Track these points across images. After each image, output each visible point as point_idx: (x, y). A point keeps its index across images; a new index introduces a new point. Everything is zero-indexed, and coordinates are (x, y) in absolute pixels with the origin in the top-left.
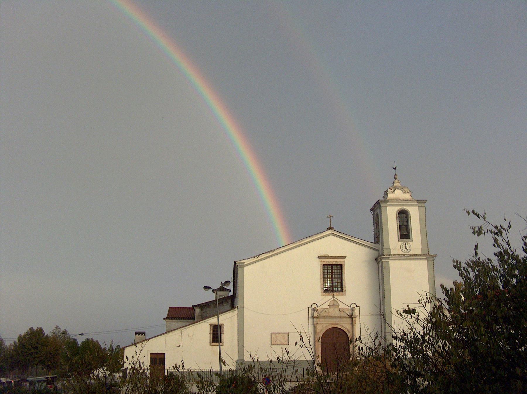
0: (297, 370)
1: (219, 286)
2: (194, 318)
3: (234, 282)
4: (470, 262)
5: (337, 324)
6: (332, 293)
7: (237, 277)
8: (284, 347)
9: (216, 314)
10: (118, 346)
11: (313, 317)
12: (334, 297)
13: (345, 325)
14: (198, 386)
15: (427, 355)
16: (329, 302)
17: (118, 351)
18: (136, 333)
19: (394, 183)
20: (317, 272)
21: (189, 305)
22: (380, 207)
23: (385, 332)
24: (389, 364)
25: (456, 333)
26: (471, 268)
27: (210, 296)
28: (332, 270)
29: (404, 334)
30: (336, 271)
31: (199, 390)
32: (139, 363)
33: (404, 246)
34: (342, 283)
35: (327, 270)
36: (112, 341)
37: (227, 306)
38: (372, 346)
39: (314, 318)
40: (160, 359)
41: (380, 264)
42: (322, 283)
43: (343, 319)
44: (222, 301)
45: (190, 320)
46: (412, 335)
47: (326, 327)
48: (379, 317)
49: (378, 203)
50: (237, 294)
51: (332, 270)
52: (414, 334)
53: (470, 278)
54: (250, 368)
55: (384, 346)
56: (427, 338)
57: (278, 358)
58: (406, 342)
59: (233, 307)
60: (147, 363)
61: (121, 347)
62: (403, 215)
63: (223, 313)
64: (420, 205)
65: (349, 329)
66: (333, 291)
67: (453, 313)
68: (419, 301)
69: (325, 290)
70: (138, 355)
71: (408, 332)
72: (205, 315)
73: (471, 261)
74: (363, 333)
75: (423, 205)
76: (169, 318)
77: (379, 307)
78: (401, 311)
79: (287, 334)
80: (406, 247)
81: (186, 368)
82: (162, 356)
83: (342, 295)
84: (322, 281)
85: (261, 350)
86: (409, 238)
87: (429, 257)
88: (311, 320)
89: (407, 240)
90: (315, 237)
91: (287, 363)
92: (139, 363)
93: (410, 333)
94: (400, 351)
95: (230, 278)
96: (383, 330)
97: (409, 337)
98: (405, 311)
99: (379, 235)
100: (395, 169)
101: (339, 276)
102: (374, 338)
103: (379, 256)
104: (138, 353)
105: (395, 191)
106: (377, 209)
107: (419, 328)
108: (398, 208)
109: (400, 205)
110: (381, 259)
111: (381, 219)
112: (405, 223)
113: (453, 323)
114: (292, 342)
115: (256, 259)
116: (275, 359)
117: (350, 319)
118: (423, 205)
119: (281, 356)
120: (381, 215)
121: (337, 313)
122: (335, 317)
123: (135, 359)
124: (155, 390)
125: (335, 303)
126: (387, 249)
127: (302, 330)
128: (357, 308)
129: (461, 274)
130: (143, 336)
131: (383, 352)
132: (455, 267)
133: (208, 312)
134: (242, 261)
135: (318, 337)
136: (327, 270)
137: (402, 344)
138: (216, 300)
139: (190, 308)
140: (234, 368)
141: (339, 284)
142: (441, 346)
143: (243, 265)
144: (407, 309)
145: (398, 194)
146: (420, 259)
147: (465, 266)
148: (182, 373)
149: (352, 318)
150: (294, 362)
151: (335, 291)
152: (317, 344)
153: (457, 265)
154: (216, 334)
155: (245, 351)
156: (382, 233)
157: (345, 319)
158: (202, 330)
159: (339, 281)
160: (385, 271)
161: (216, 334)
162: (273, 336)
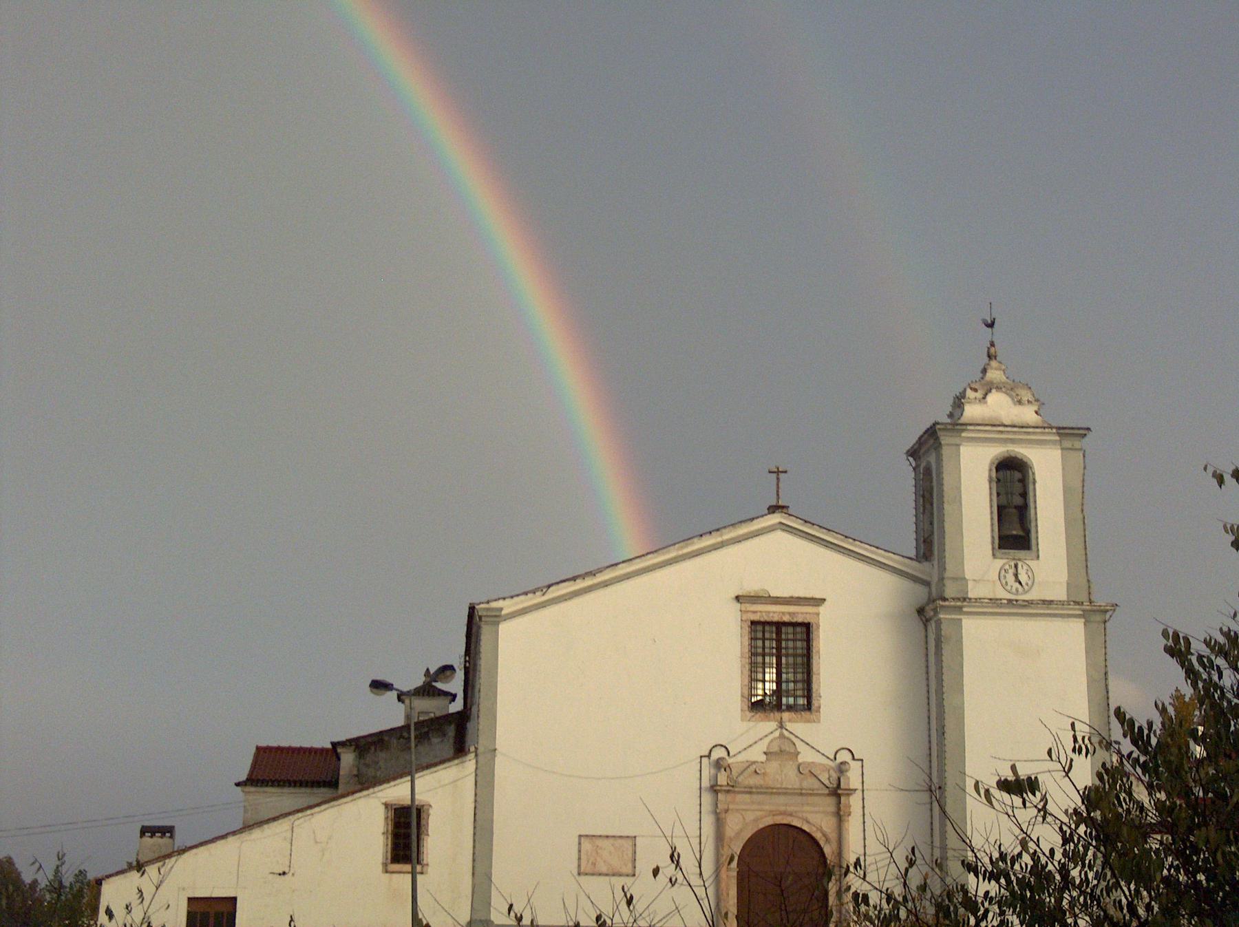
1: (419, 681)
4: (1222, 639)
5: (791, 815)
6: (778, 715)
7: (478, 653)
8: (618, 882)
9: (408, 771)
11: (714, 789)
12: (781, 726)
13: (815, 818)
16: (767, 740)
17: (81, 890)
18: (144, 831)
19: (984, 371)
20: (731, 643)
21: (322, 741)
22: (938, 446)
23: (944, 848)
26: (1226, 656)
27: (389, 714)
28: (779, 641)
29: (1003, 857)
30: (791, 644)
33: (1012, 571)
34: (808, 682)
35: (764, 639)
36: (61, 857)
37: (443, 745)
38: (898, 891)
39: (716, 792)
40: (219, 916)
42: (746, 681)
43: (810, 799)
45: (323, 790)
46: (1026, 858)
47: (756, 820)
48: (925, 797)
50: (474, 709)
51: (779, 641)
52: (1034, 856)
53: (1222, 689)
55: (938, 892)
57: (598, 918)
58: (1009, 882)
59: (460, 749)
61: (91, 876)
62: (1012, 476)
63: (428, 767)
64: (1068, 443)
66: (778, 707)
67: (1162, 796)
68: (1050, 752)
69: (753, 704)
70: (146, 903)
71: (1016, 852)
72: (371, 772)
73: (1227, 634)
74: (874, 843)
77: (925, 766)
78: (992, 782)
79: (630, 842)
80: (1016, 575)
82: (224, 908)
83: (808, 721)
84: (747, 673)
87: (1094, 612)
88: (707, 798)
90: (728, 535)
93: (1020, 855)
94: (987, 911)
96: (937, 843)
97: (1017, 867)
98: (1004, 785)
99: (932, 533)
102: (903, 865)
103: (931, 600)
105: (990, 398)
106: (927, 451)
107: (1048, 837)
108: (994, 452)
109: (1006, 441)
111: (941, 484)
112: (1018, 501)
113: (1161, 827)
114: (644, 868)
115: (538, 598)
117: (831, 801)
118: (1077, 444)
119: (607, 911)
120: (940, 473)
121: (787, 776)
122: (784, 792)
125: (787, 747)
126: (955, 579)
127: (678, 831)
128: (855, 766)
129: (1191, 674)
131: (931, 910)
132: (1171, 651)
133: (381, 764)
134: (494, 605)
135: (726, 853)
136: (764, 639)
137: (993, 888)
138: (406, 727)
139: (323, 750)
141: (800, 685)
142: (1124, 901)
143: (497, 618)
144: (1011, 778)
145: (998, 406)
147: (1205, 651)
149: (839, 796)
151: (790, 708)
152: (723, 874)
153: (1177, 649)
154: (405, 836)
155: (494, 892)
156: (942, 528)
157: (816, 799)
158: (362, 818)
159: (799, 676)
161: (405, 836)
162: (586, 845)
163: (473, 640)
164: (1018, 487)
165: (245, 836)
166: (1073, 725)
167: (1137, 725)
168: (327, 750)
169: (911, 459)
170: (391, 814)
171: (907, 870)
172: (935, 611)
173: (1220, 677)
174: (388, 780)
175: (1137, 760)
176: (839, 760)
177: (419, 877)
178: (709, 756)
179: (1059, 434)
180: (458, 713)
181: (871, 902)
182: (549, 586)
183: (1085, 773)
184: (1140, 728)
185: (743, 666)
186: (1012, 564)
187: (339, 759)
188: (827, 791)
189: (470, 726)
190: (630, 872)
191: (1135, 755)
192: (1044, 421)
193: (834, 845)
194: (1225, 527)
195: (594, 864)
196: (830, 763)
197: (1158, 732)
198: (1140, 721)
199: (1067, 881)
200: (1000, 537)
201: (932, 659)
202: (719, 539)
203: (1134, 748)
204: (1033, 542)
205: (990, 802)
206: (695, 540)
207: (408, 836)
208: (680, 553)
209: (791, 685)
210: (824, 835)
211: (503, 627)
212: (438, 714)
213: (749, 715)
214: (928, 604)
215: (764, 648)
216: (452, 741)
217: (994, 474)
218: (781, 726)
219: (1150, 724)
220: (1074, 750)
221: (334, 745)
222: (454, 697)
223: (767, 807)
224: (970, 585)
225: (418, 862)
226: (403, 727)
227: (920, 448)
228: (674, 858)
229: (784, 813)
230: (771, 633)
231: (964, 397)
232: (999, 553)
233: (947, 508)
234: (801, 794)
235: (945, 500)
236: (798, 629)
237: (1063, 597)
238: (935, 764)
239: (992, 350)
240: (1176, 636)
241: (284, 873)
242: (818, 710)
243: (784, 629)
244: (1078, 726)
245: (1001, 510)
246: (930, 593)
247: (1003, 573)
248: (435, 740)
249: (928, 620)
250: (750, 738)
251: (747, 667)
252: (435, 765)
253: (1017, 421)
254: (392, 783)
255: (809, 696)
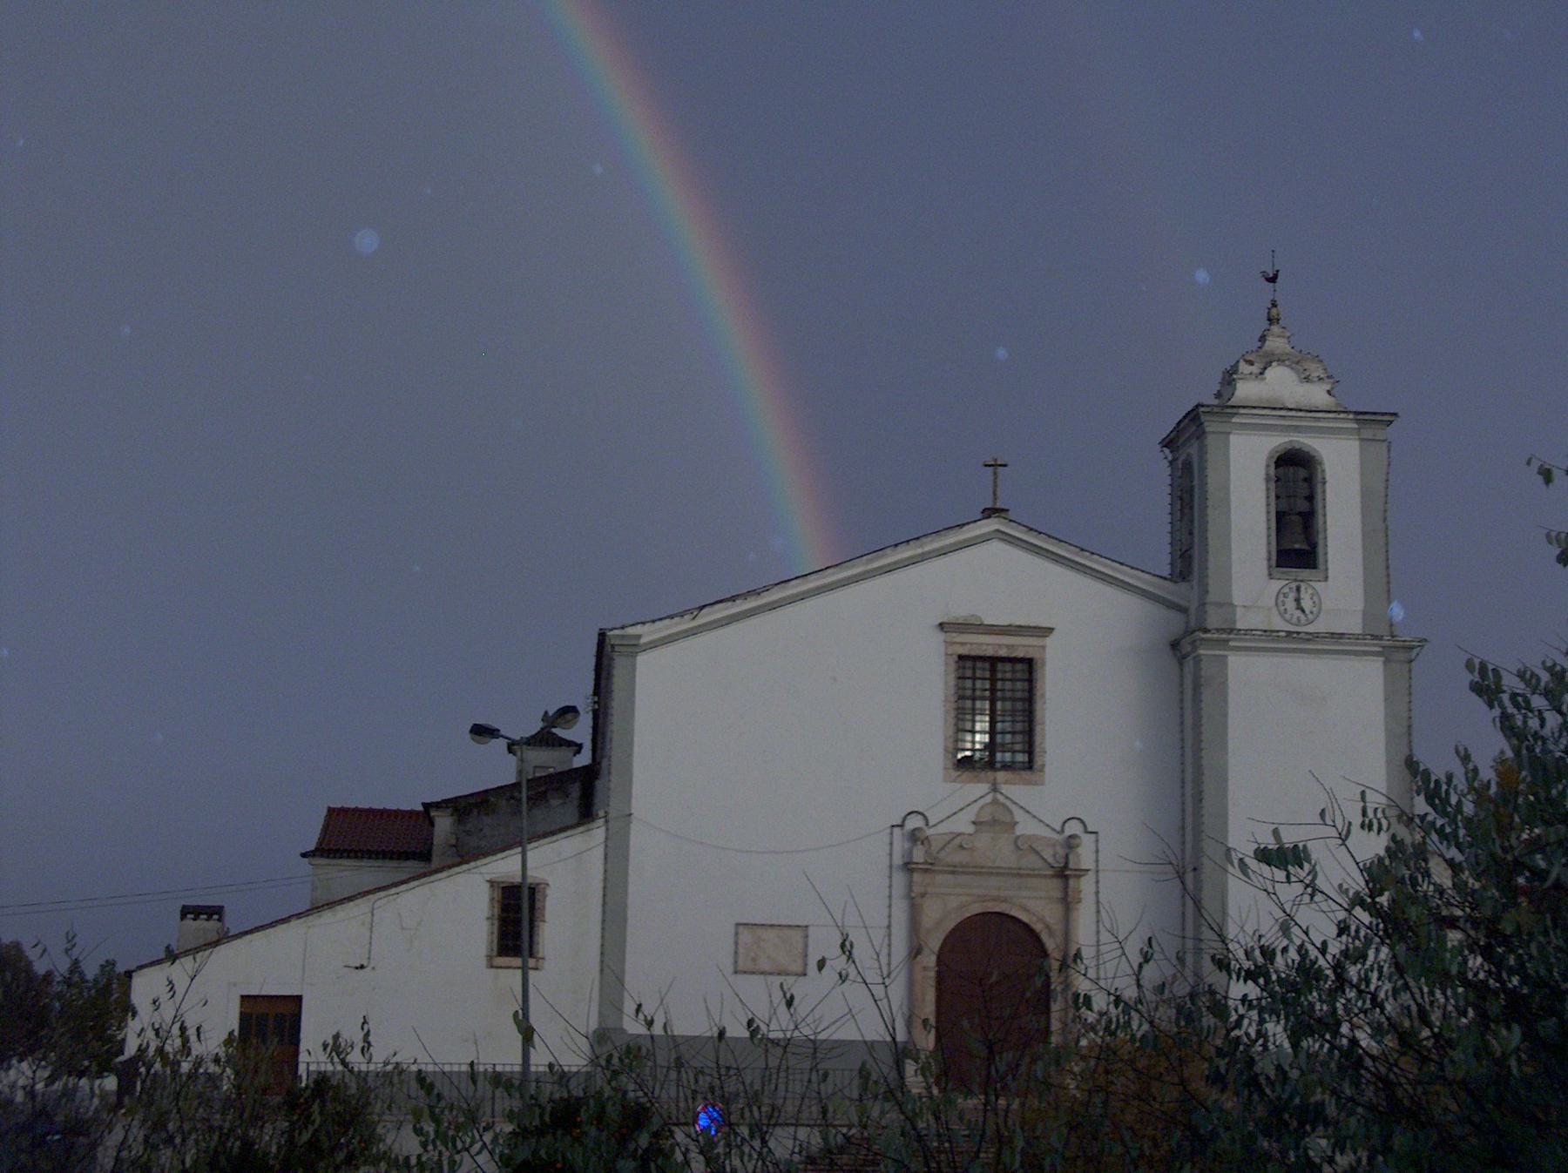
0: (826, 1075)
1: (535, 726)
2: (425, 855)
3: (596, 715)
5: (1005, 901)
6: (990, 774)
9: (518, 841)
10: (111, 964)
11: (908, 867)
12: (995, 789)
13: (1034, 906)
14: (418, 1131)
15: (1354, 1042)
18: (185, 912)
19: (1263, 339)
20: (933, 683)
21: (412, 802)
22: (1201, 435)
24: (1197, 1070)
25: (1476, 962)
27: (495, 768)
30: (1008, 685)
31: (424, 1145)
32: (183, 1029)
33: (1292, 596)
34: (1029, 733)
35: (974, 679)
37: (567, 809)
38: (1130, 993)
39: (911, 871)
41: (1189, 663)
42: (951, 730)
44: (543, 788)
45: (410, 863)
49: (1193, 418)
50: (604, 764)
51: (993, 680)
54: (634, 1053)
56: (1353, 972)
57: (750, 1022)
59: (586, 814)
60: (216, 1024)
62: (1295, 474)
63: (545, 835)
64: (1368, 433)
65: (1051, 921)
66: (991, 765)
70: (178, 997)
74: (1110, 943)
75: (1380, 435)
76: (326, 849)
78: (1249, 849)
80: (1298, 600)
81: (379, 1054)
83: (1029, 783)
84: (952, 721)
85: (690, 990)
86: (1315, 567)
87: (1396, 650)
88: (899, 879)
89: (1304, 573)
90: (931, 545)
91: (785, 1045)
92: (183, 1029)
95: (581, 696)
98: (1264, 855)
99: (1191, 547)
100: (1272, 279)
101: (1019, 705)
102: (1136, 959)
103: (1189, 632)
104: (180, 992)
105: (1269, 373)
106: (1187, 440)
107: (1320, 925)
108: (1275, 442)
110: (1193, 643)
111: (1204, 484)
112: (1302, 505)
115: (686, 624)
116: (737, 1031)
117: (1056, 883)
119: (762, 1013)
120: (1203, 469)
121: (1000, 852)
123: (168, 1012)
124: (247, 1144)
126: (1220, 605)
128: (1087, 840)
130: (213, 925)
132: (1477, 689)
134: (630, 631)
137: (1252, 990)
138: (516, 786)
139: (411, 813)
140: (574, 1059)
142: (1414, 1008)
143: (635, 647)
144: (1273, 846)
145: (1281, 384)
146: (1356, 653)
147: (1520, 687)
148: (362, 1077)
149: (1066, 878)
150: (815, 1046)
151: (1006, 767)
153: (1486, 686)
154: (516, 922)
158: (460, 899)
160: (1207, 695)
161: (516, 922)
163: (604, 674)
164: (1303, 489)
165: (313, 920)
166: (1363, 793)
167: (1433, 778)
168: (418, 813)
169: (1167, 451)
170: (498, 894)
171: (1141, 966)
172: (1195, 648)
173: (1542, 725)
174: (494, 853)
175: (1433, 823)
176: (1068, 833)
177: (531, 972)
178: (901, 826)
179: (1357, 421)
180: (585, 767)
181: (1096, 1007)
182: (701, 608)
183: (1372, 846)
184: (1437, 782)
185: (947, 712)
186: (1294, 585)
187: (432, 825)
188: (1050, 872)
189: (599, 784)
190: (800, 969)
191: (1430, 818)
192: (1338, 405)
193: (1059, 939)
194: (1548, 535)
195: (754, 960)
196: (1056, 836)
197: (1460, 787)
198: (1438, 773)
199: (1341, 980)
200: (1279, 552)
201: (1188, 704)
202: (920, 551)
203: (1429, 809)
204: (1321, 559)
205: (1245, 873)
206: (888, 551)
207: (518, 922)
208: (870, 567)
209: (1008, 737)
210: (1048, 927)
211: (642, 659)
212: (559, 769)
213: (955, 774)
214: (1184, 637)
215: (974, 690)
216: (576, 803)
217: (1272, 471)
218: (995, 789)
219: (1450, 778)
220: (1362, 826)
221: (427, 806)
222: (579, 747)
223: (975, 891)
224: (1239, 611)
225: (531, 955)
226: (514, 785)
227: (1178, 436)
228: (846, 947)
229: (995, 899)
230: (983, 671)
231: (1236, 372)
232: (1277, 571)
233: (1212, 513)
234: (1019, 875)
235: (1210, 503)
236: (1019, 666)
237: (1358, 630)
238: (1189, 838)
239: (1274, 311)
240: (1483, 668)
241: (362, 967)
242: (1042, 770)
243: (1000, 666)
244: (1370, 796)
245: (1280, 516)
246: (1187, 623)
247: (1281, 598)
248: (555, 802)
249: (1184, 657)
250: (955, 805)
251: (953, 714)
252: (553, 833)
253: (1304, 403)
254: (500, 856)
255: (1030, 751)
